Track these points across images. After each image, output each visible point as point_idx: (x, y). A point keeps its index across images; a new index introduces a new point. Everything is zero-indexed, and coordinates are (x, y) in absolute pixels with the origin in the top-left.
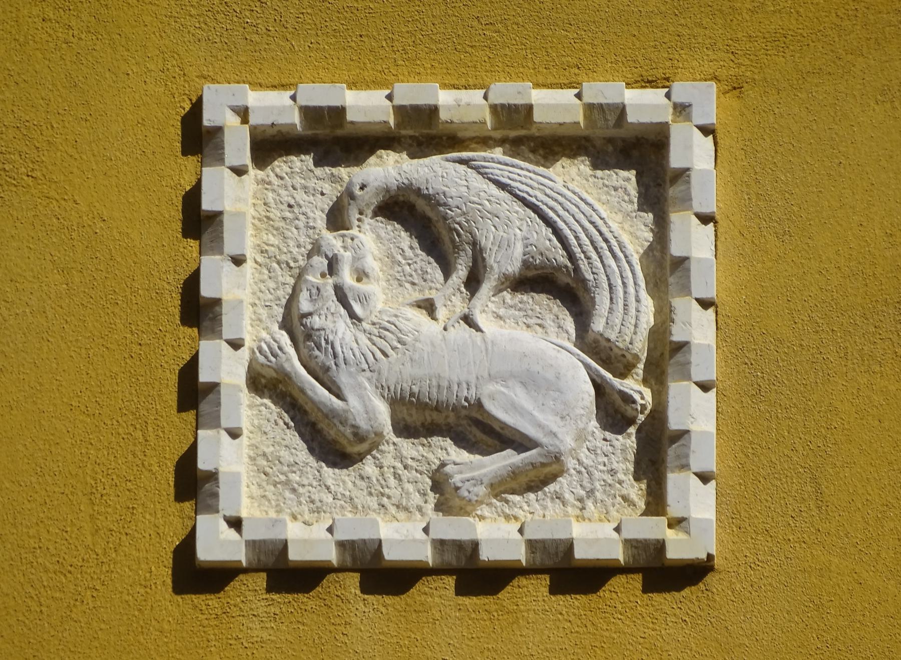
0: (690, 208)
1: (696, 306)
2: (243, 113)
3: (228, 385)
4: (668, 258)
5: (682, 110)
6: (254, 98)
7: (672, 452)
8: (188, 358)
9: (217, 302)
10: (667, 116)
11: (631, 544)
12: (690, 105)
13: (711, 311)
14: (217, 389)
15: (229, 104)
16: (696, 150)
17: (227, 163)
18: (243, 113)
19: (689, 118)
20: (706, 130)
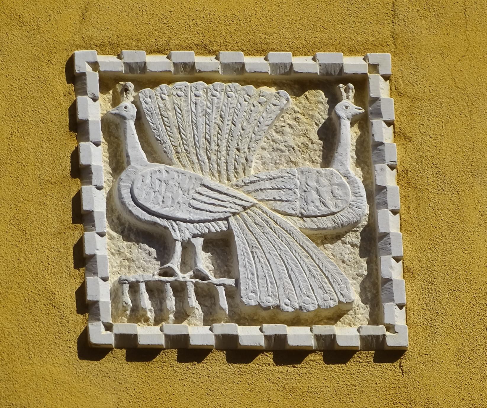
2: (95, 65)
4: (380, 279)
5: (374, 68)
6: (101, 59)
7: (380, 244)
8: (79, 238)
9: (97, 302)
12: (378, 65)
14: (96, 305)
15: (88, 60)
17: (93, 184)
18: (95, 65)
20: (386, 78)
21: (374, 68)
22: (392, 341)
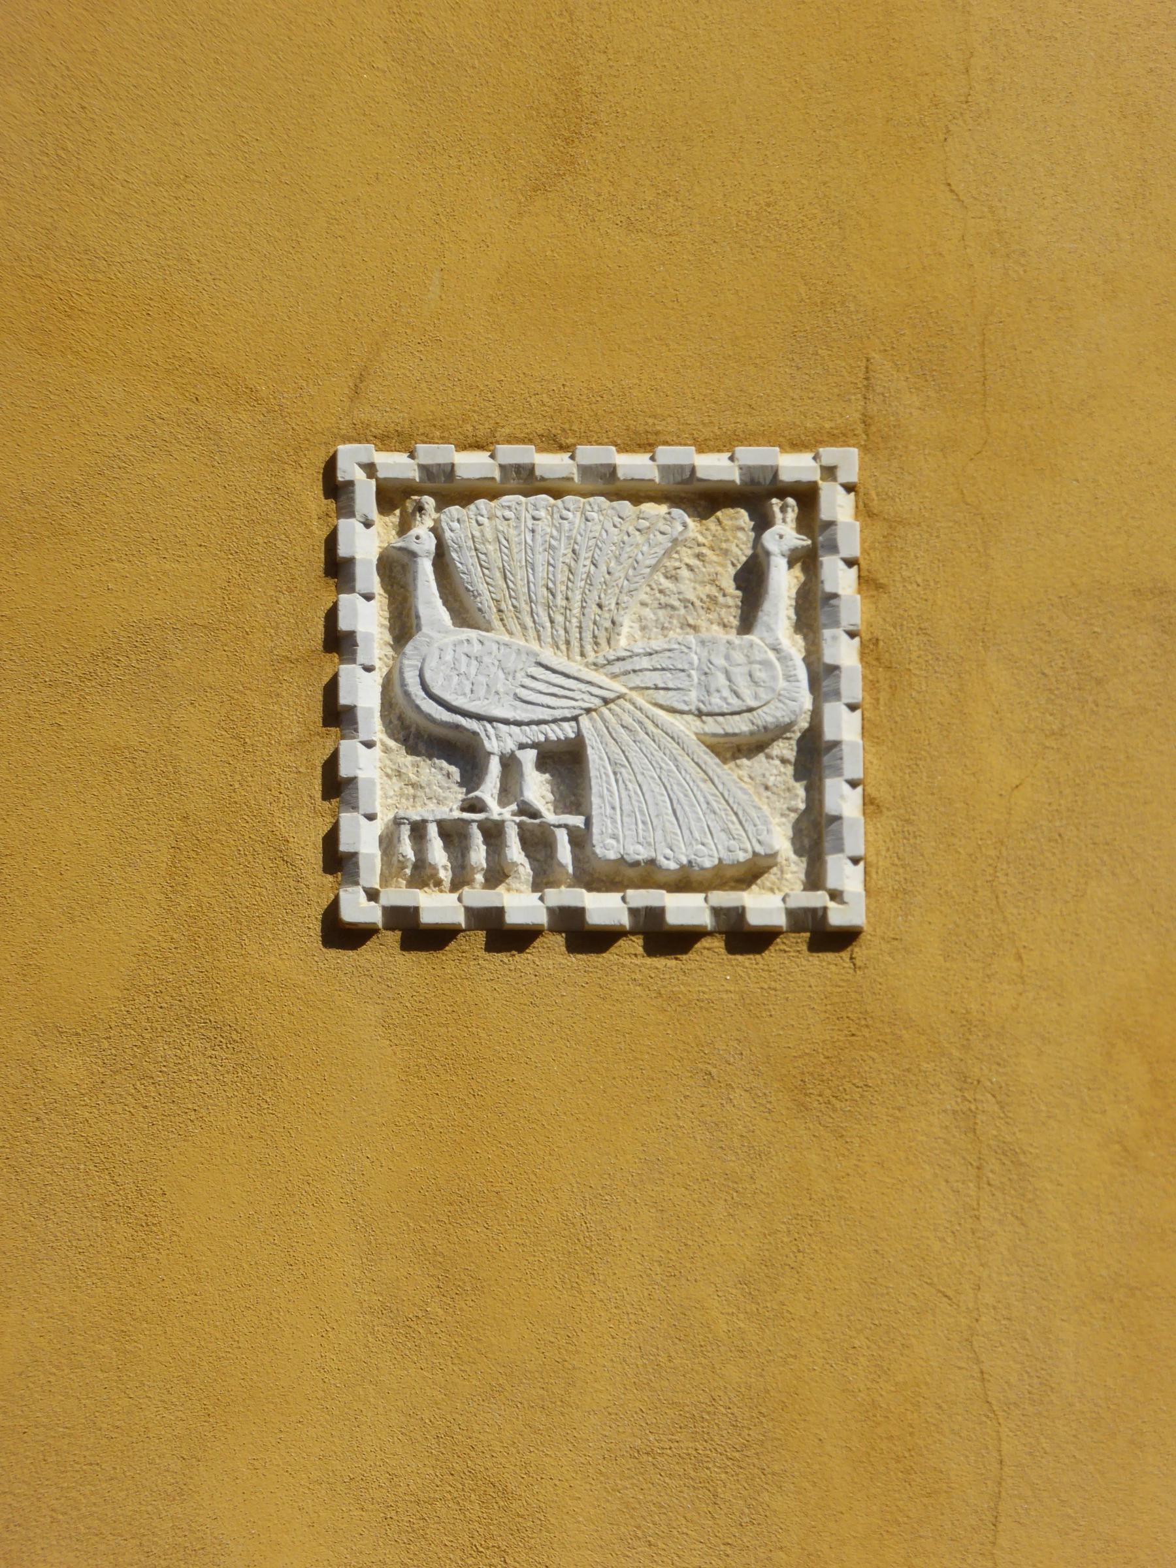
0: (841, 775)
1: (841, 490)
2: (370, 469)
3: (364, 708)
5: (830, 472)
7: (826, 759)
9: (354, 855)
10: (816, 476)
11: (791, 913)
13: (855, 569)
16: (844, 726)
18: (370, 469)
19: (835, 479)
20: (849, 488)
21: (830, 472)
22: (838, 917)
